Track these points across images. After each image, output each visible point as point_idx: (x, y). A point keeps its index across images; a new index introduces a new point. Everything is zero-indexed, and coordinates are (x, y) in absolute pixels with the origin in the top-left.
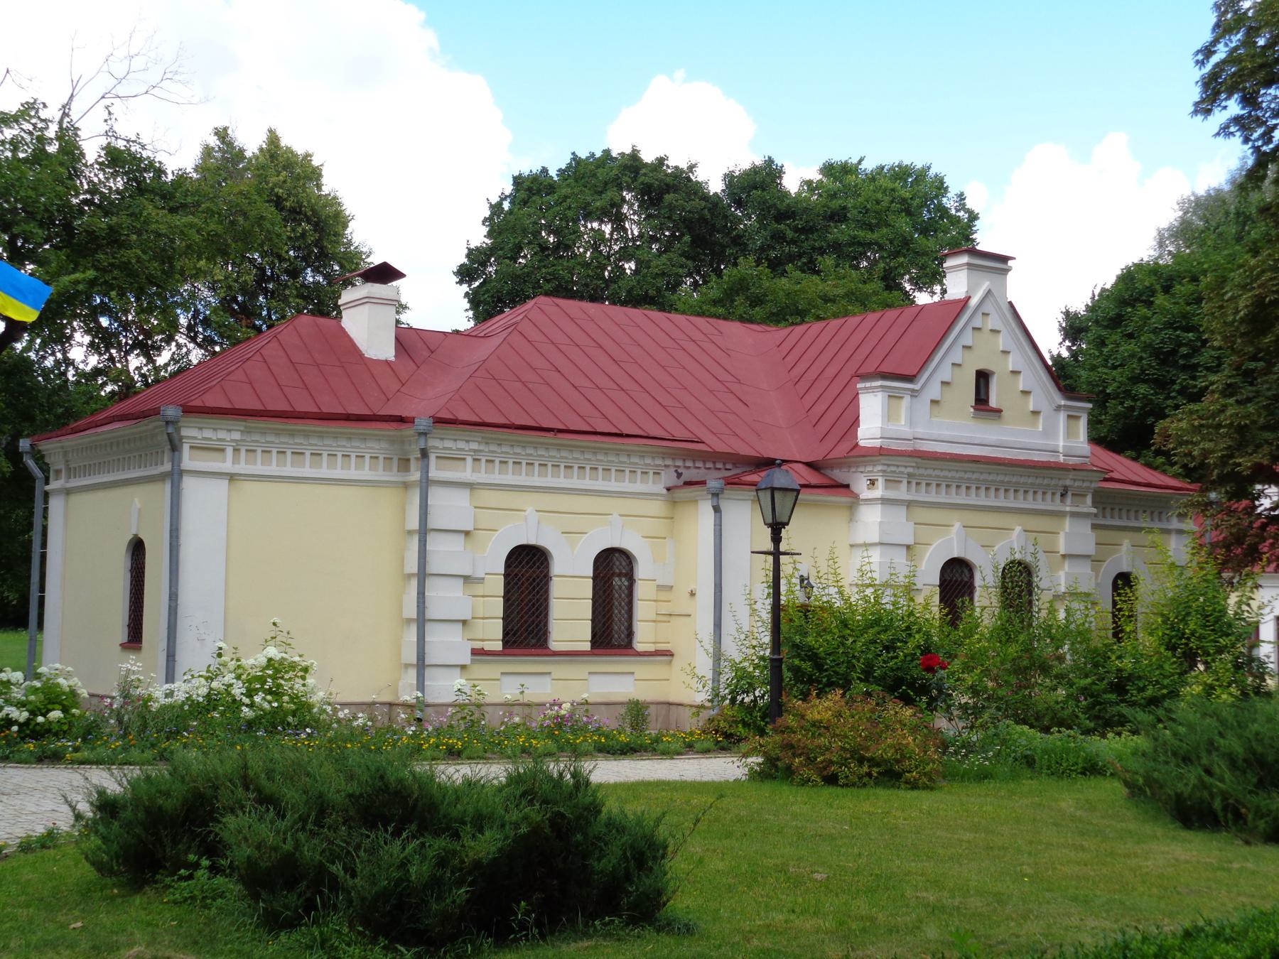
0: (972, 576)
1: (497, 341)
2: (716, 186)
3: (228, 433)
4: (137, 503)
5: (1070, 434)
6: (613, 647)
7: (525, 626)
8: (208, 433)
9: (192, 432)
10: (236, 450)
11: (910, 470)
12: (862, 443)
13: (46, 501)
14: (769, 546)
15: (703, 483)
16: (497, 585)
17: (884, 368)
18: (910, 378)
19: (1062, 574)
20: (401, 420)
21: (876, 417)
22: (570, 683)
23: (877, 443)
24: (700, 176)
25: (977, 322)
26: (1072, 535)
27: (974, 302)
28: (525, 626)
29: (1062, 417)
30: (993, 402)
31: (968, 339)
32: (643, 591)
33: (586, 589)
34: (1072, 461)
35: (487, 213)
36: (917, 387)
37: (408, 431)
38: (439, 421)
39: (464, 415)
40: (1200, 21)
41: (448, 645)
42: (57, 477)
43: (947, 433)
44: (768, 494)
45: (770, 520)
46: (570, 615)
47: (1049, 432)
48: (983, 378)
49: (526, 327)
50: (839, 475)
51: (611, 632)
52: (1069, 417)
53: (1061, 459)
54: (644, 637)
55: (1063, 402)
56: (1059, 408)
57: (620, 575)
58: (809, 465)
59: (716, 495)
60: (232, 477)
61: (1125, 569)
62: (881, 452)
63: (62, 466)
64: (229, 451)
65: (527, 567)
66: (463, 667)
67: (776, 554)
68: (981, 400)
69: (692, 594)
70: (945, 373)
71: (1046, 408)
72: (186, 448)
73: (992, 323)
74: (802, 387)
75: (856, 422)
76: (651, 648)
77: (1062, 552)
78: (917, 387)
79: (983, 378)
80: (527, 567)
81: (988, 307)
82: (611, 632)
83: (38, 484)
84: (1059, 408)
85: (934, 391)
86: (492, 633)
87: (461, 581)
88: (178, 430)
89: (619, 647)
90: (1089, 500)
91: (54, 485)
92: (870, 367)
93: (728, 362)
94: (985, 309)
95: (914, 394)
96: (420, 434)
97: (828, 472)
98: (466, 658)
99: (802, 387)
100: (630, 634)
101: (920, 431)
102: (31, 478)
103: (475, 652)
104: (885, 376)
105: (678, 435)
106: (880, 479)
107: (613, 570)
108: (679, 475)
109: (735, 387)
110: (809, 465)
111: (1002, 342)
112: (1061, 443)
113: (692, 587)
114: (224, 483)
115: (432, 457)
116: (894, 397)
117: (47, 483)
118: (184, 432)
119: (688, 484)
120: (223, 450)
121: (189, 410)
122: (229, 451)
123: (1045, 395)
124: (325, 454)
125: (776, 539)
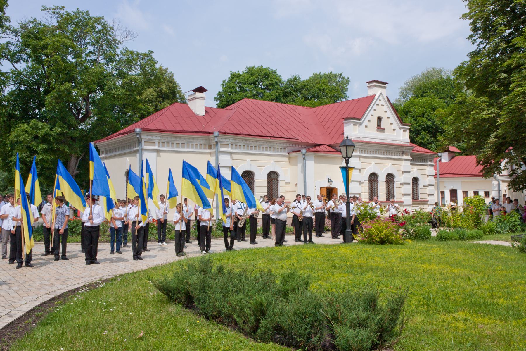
1: (235, 110)
3: (156, 137)
8: (150, 137)
9: (145, 137)
10: (159, 143)
11: (360, 147)
15: (300, 151)
18: (359, 119)
20: (209, 133)
25: (377, 103)
26: (406, 165)
27: (376, 97)
30: (382, 127)
31: (375, 107)
32: (281, 184)
36: (361, 122)
37: (211, 136)
38: (221, 133)
39: (228, 131)
42: (103, 154)
43: (366, 135)
48: (379, 119)
49: (242, 106)
52: (404, 131)
55: (402, 126)
58: (328, 145)
59: (304, 154)
60: (158, 151)
61: (415, 176)
63: (104, 150)
65: (373, 177)
68: (379, 126)
70: (369, 117)
71: (397, 128)
72: (143, 142)
78: (361, 122)
79: (379, 119)
80: (373, 177)
81: (381, 98)
82: (272, 196)
84: (401, 128)
85: (366, 123)
87: (358, 183)
88: (140, 136)
93: (299, 117)
94: (380, 99)
96: (215, 137)
105: (290, 137)
107: (273, 178)
109: (304, 124)
113: (296, 182)
114: (155, 154)
115: (219, 144)
118: (142, 137)
120: (154, 143)
121: (143, 130)
124: (186, 144)
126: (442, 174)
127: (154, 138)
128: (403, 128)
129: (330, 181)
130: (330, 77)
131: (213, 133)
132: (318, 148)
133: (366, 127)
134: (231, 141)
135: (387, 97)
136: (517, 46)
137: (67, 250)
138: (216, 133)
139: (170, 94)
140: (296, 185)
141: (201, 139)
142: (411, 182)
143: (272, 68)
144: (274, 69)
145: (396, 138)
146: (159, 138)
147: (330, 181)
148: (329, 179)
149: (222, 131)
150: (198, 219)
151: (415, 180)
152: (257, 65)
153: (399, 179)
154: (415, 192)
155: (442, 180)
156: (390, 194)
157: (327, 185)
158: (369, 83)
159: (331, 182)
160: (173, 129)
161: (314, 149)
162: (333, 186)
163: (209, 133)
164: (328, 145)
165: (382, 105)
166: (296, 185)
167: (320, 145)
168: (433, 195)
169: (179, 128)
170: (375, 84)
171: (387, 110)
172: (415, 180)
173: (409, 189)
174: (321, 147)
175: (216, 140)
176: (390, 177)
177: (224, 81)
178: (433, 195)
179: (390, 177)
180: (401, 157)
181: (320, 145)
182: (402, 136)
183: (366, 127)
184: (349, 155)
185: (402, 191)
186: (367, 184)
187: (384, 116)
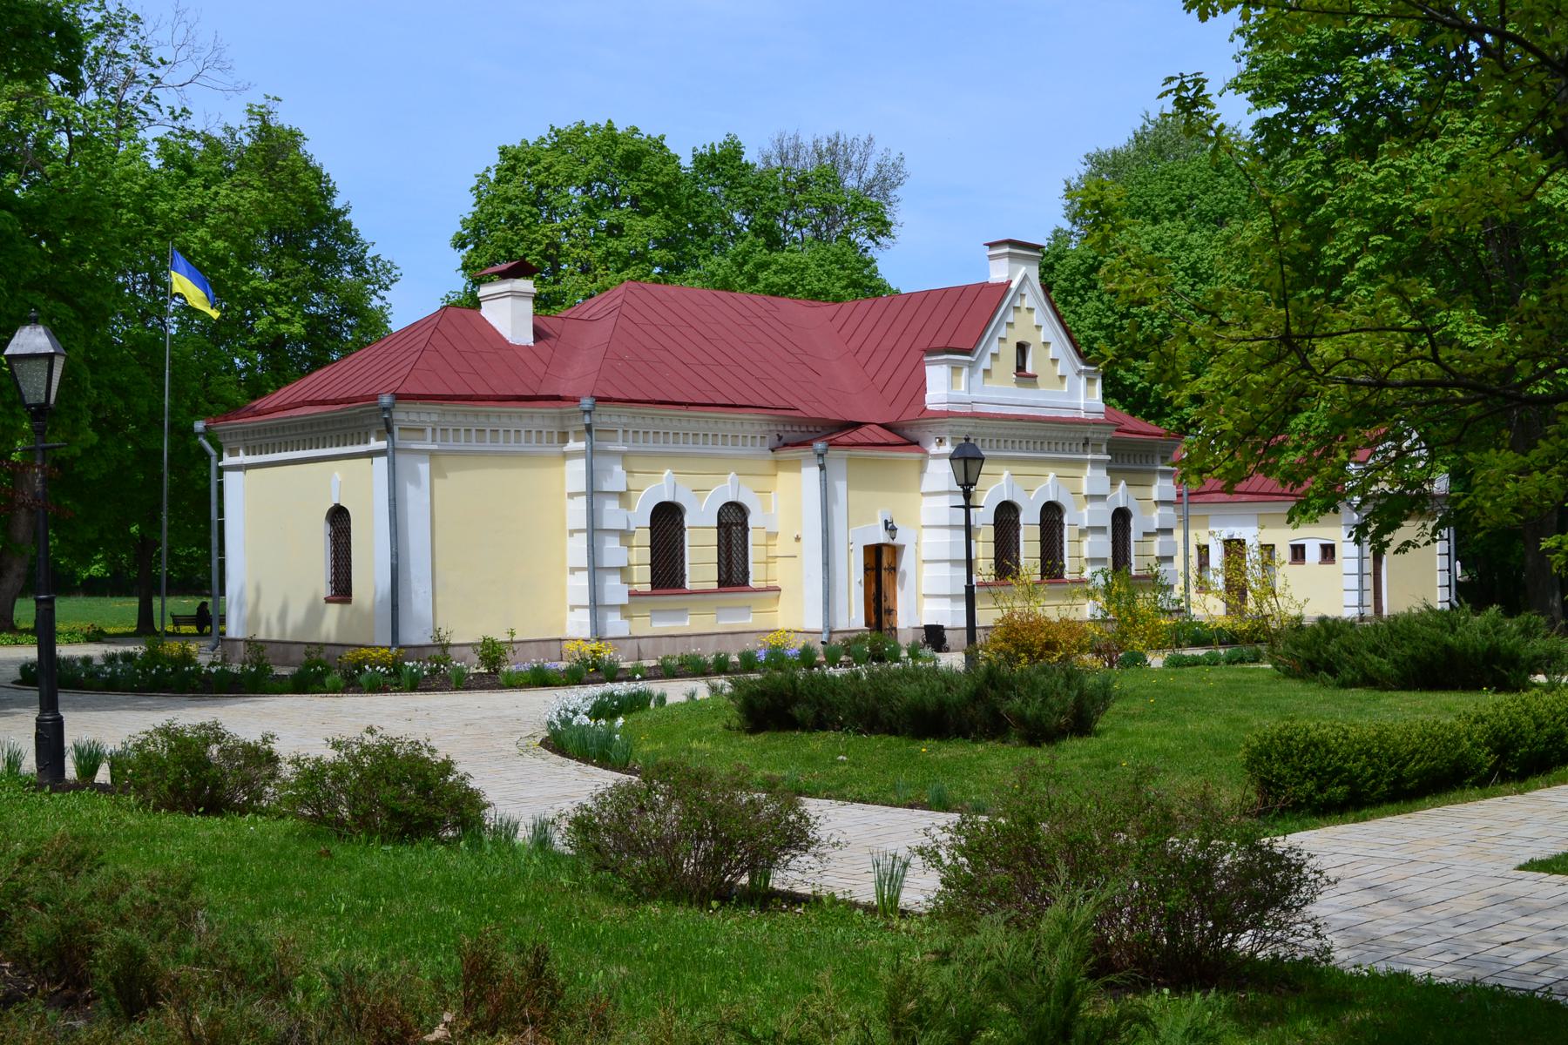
0: (1061, 517)
3: (427, 415)
4: (338, 476)
5: (1087, 394)
7: (667, 570)
8: (413, 417)
12: (929, 407)
13: (220, 476)
14: (962, 502)
16: (644, 537)
17: (935, 344)
18: (967, 352)
19: (1085, 511)
21: (942, 386)
22: (702, 622)
23: (944, 407)
24: (672, 146)
26: (1092, 478)
27: (1014, 286)
28: (667, 570)
29: (1083, 380)
30: (1029, 369)
32: (753, 537)
34: (1091, 417)
35: (474, 183)
37: (568, 408)
38: (599, 400)
39: (615, 395)
41: (616, 593)
43: (995, 397)
46: (700, 558)
47: (1073, 392)
48: (1022, 348)
50: (914, 434)
51: (733, 572)
53: (1083, 415)
54: (756, 577)
56: (1079, 373)
58: (881, 425)
59: (821, 455)
64: (429, 431)
65: (667, 518)
66: (622, 607)
67: (967, 507)
68: (1021, 368)
69: (798, 539)
71: (1070, 373)
73: (1026, 303)
76: (763, 585)
77: (1085, 492)
79: (1022, 348)
80: (667, 518)
83: (213, 460)
84: (1079, 373)
85: (986, 363)
86: (642, 576)
90: (1104, 448)
91: (228, 460)
95: (971, 365)
97: (907, 432)
98: (625, 600)
100: (746, 573)
101: (976, 395)
102: (203, 455)
103: (632, 594)
106: (948, 438)
107: (733, 521)
108: (780, 438)
109: (805, 358)
110: (886, 427)
111: (1035, 318)
112: (1082, 402)
116: (956, 369)
117: (220, 458)
119: (786, 445)
120: (423, 430)
122: (429, 431)
123: (1068, 362)
126: (1188, 502)
127: (424, 417)
128: (1086, 372)
129: (890, 527)
131: (576, 400)
132: (855, 436)
133: (987, 372)
134: (624, 420)
136: (1176, 403)
138: (586, 403)
141: (540, 417)
142: (1108, 523)
143: (649, 129)
144: (655, 135)
146: (435, 418)
147: (890, 527)
148: (886, 523)
151: (1121, 517)
153: (1078, 516)
155: (1194, 511)
157: (882, 537)
158: (991, 245)
159: (894, 529)
160: (468, 392)
161: (844, 439)
162: (897, 541)
164: (881, 425)
165: (1030, 310)
167: (857, 425)
168: (339, 518)
169: (483, 391)
170: (1007, 250)
171: (1043, 322)
172: (1121, 517)
173: (1102, 546)
174: (863, 430)
175: (587, 420)
176: (1052, 514)
177: (483, 178)
178: (339, 518)
179: (1052, 514)
180: (362, 448)
181: (857, 425)
182: (1083, 397)
183: (987, 372)
184: (971, 480)
185: (1085, 551)
187: (1035, 340)
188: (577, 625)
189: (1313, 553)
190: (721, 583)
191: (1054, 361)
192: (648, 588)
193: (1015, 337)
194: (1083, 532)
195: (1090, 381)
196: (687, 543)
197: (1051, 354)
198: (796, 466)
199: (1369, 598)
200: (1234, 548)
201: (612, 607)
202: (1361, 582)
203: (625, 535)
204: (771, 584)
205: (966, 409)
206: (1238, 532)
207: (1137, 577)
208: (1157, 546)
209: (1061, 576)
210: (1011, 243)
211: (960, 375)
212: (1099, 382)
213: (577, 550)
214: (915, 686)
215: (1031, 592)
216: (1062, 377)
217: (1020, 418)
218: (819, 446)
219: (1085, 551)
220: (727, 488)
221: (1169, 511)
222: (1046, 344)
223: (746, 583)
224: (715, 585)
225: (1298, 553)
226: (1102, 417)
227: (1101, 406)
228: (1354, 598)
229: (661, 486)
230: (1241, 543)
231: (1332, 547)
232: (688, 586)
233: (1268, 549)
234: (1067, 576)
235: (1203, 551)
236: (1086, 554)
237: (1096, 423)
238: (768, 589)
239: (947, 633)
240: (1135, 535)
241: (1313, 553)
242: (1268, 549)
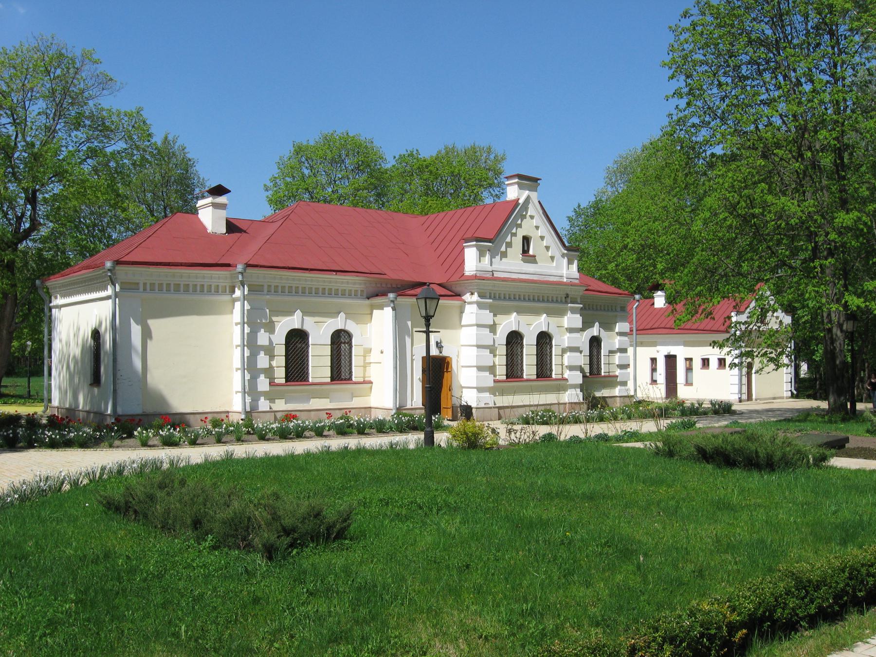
2: (389, 163)
6: (342, 380)
20: (229, 265)
21: (472, 260)
22: (316, 404)
29: (565, 260)
30: (531, 252)
33: (328, 351)
40: (688, 1)
43: (508, 268)
44: (423, 301)
45: (424, 314)
46: (319, 364)
47: (558, 267)
48: (526, 240)
50: (458, 289)
51: (340, 370)
53: (565, 280)
57: (344, 343)
58: (439, 285)
59: (393, 301)
62: (475, 277)
68: (525, 251)
71: (558, 255)
74: (435, 245)
75: (463, 262)
77: (566, 326)
79: (526, 240)
80: (297, 340)
86: (280, 374)
89: (345, 380)
91: (55, 302)
92: (469, 235)
97: (454, 289)
99: (435, 245)
101: (495, 267)
104: (478, 240)
107: (340, 341)
111: (534, 222)
112: (565, 272)
117: (51, 302)
121: (118, 262)
123: (556, 249)
125: (428, 325)
130: (473, 154)
135: (539, 202)
137: (300, 327)
139: (177, 189)
140: (382, 352)
141: (218, 276)
145: (554, 272)
148: (437, 343)
149: (250, 263)
150: (434, 352)
151: (595, 342)
152: (340, 131)
153: (561, 340)
154: (595, 360)
156: (543, 370)
162: (445, 353)
163: (229, 265)
164: (439, 285)
166: (382, 352)
170: (516, 180)
171: (540, 224)
172: (595, 342)
173: (582, 360)
176: (544, 339)
179: (544, 339)
182: (565, 270)
185: (568, 363)
186: (502, 350)
187: (535, 235)
188: (234, 404)
189: (714, 363)
190: (538, 376)
191: (547, 248)
192: (504, 378)
193: (521, 233)
194: (564, 351)
195: (570, 262)
196: (310, 354)
197: (545, 243)
198: (381, 307)
199: (745, 389)
200: (671, 360)
201: (574, 386)
202: (741, 380)
203: (270, 351)
204: (367, 379)
205: (489, 275)
206: (673, 350)
207: (604, 376)
208: (617, 359)
209: (550, 376)
210: (520, 177)
211: (572, 264)
212: (576, 262)
213: (236, 358)
214: (722, 423)
215: (319, 390)
216: (552, 258)
217: (514, 280)
218: (391, 296)
219: (568, 363)
220: (339, 322)
221: (625, 339)
222: (542, 238)
223: (350, 379)
224: (329, 380)
225: (705, 363)
226: (577, 281)
227: (576, 275)
228: (736, 389)
229: (294, 321)
230: (675, 357)
231: (708, 360)
232: (310, 380)
233: (689, 360)
234: (554, 376)
235: (654, 361)
236: (566, 363)
237: (572, 285)
238: (364, 382)
239: (474, 411)
240: (604, 352)
241: (714, 363)
242: (689, 360)
